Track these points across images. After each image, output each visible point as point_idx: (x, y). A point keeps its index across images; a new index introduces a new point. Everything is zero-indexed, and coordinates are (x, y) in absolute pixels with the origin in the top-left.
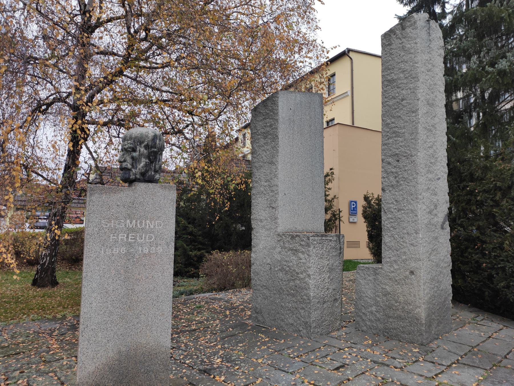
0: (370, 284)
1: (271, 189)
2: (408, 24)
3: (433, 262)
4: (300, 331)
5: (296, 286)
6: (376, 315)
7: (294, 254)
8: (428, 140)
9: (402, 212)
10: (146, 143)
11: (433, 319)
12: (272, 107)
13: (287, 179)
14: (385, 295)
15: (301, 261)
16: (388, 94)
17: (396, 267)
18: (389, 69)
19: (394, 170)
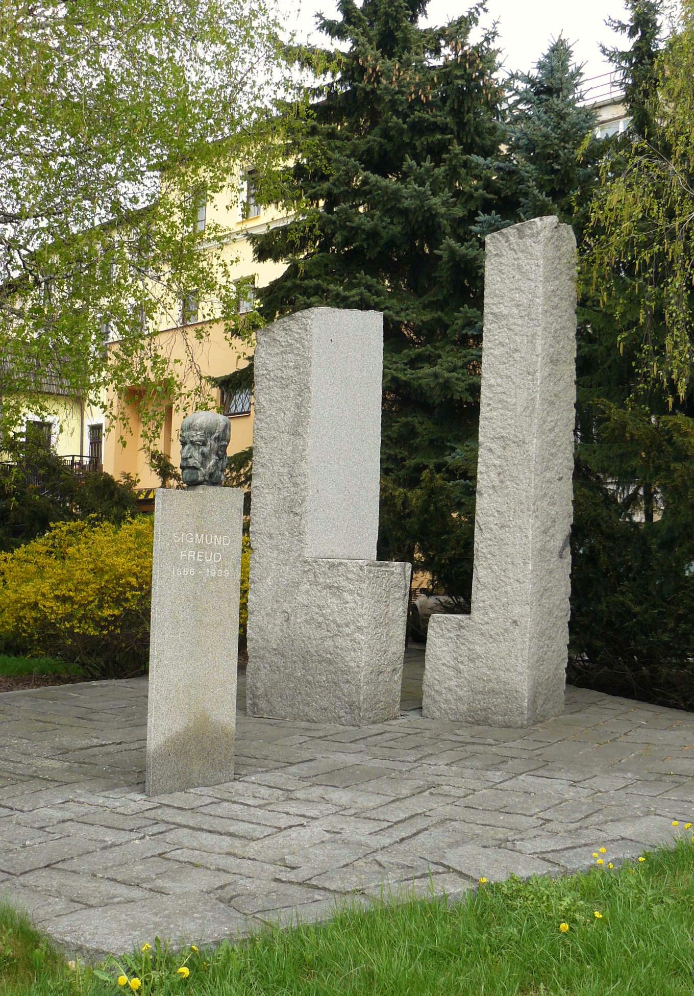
0: (450, 645)
1: (293, 480)
2: (528, 232)
3: (545, 607)
4: (340, 718)
5: (337, 647)
6: (456, 692)
7: (334, 594)
8: (549, 419)
9: (507, 529)
10: (216, 434)
11: (540, 693)
12: (298, 333)
13: (322, 464)
14: (472, 660)
15: (347, 605)
16: (494, 335)
17: (492, 615)
18: (496, 296)
19: (497, 462)
